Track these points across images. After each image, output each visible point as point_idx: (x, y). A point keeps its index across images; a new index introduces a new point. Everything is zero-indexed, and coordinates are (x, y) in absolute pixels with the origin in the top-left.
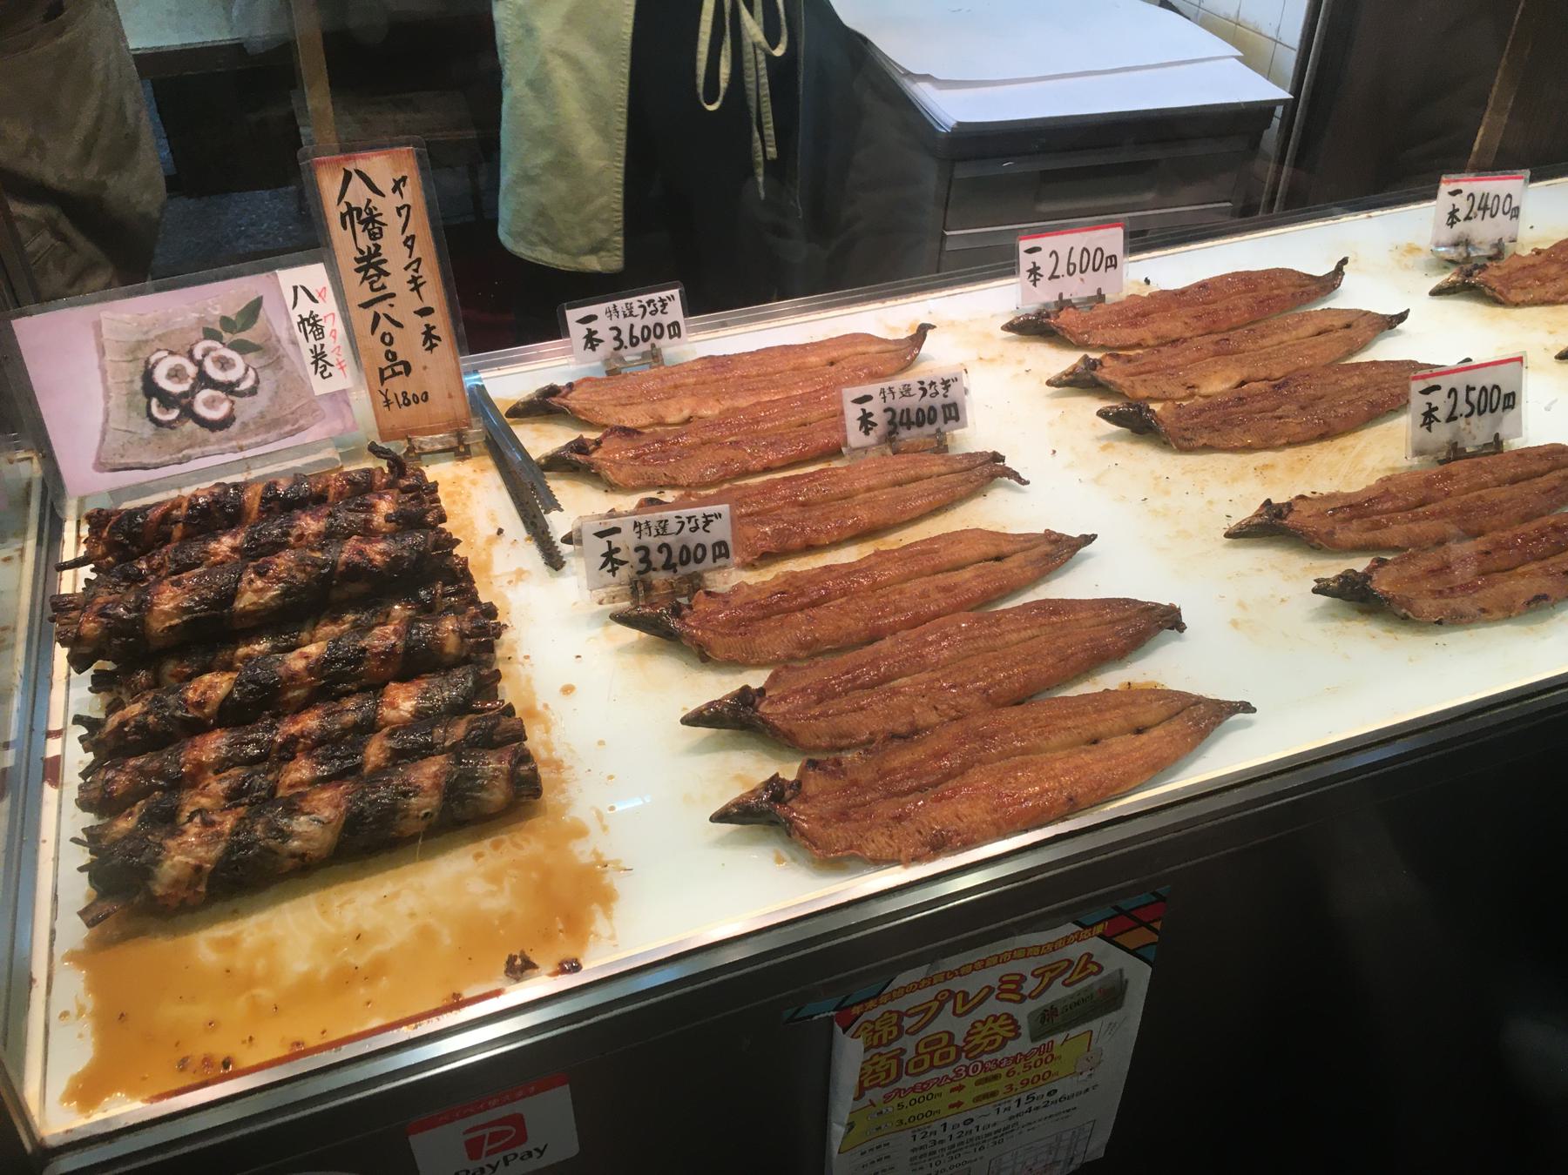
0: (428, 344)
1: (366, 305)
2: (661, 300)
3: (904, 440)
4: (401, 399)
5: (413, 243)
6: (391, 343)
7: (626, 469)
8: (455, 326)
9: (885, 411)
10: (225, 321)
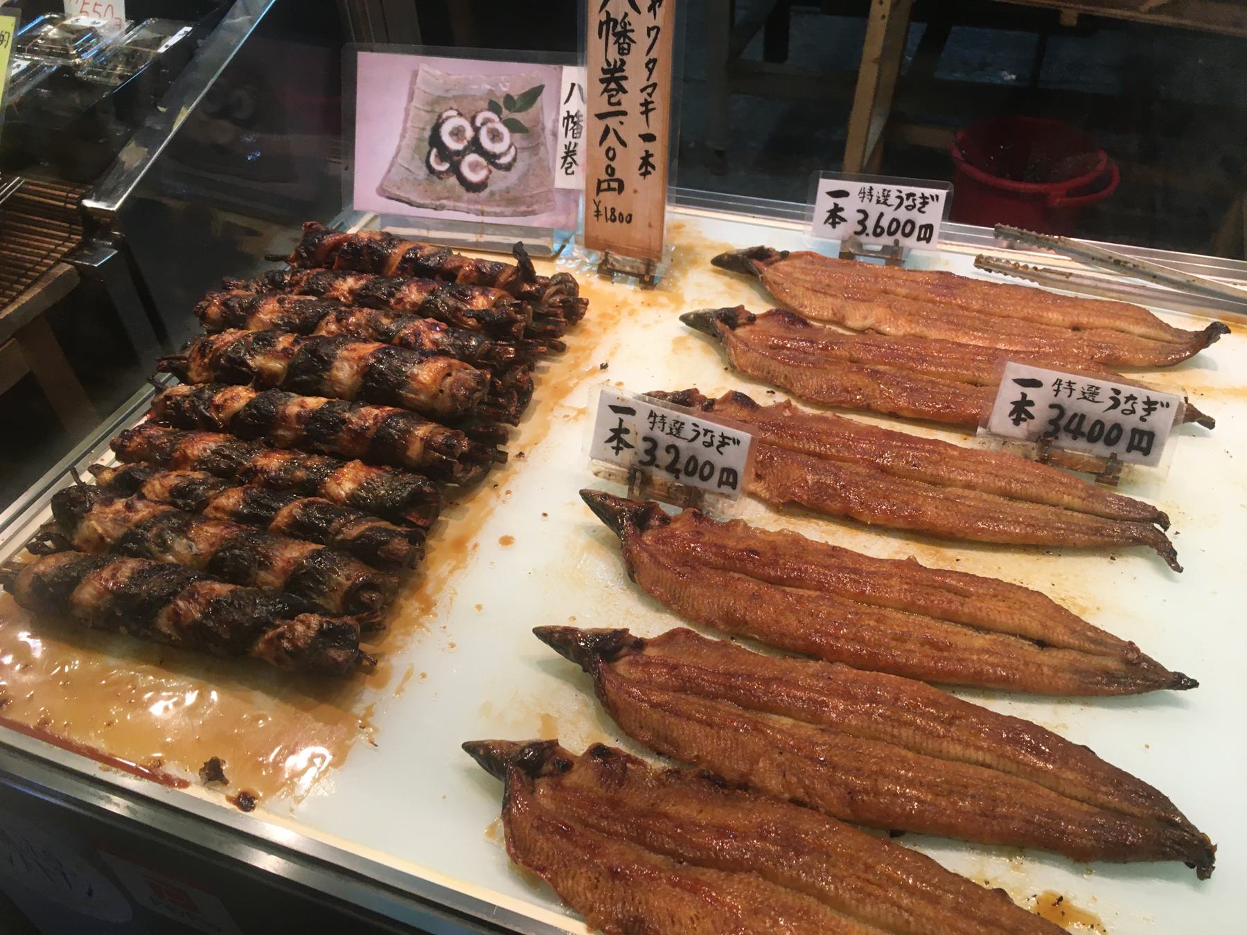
0: (643, 170)
1: (601, 116)
2: (923, 197)
3: (1062, 449)
4: (609, 214)
5: (653, 66)
6: (612, 159)
7: (753, 355)
8: (671, 160)
9: (1052, 406)
10: (508, 98)
